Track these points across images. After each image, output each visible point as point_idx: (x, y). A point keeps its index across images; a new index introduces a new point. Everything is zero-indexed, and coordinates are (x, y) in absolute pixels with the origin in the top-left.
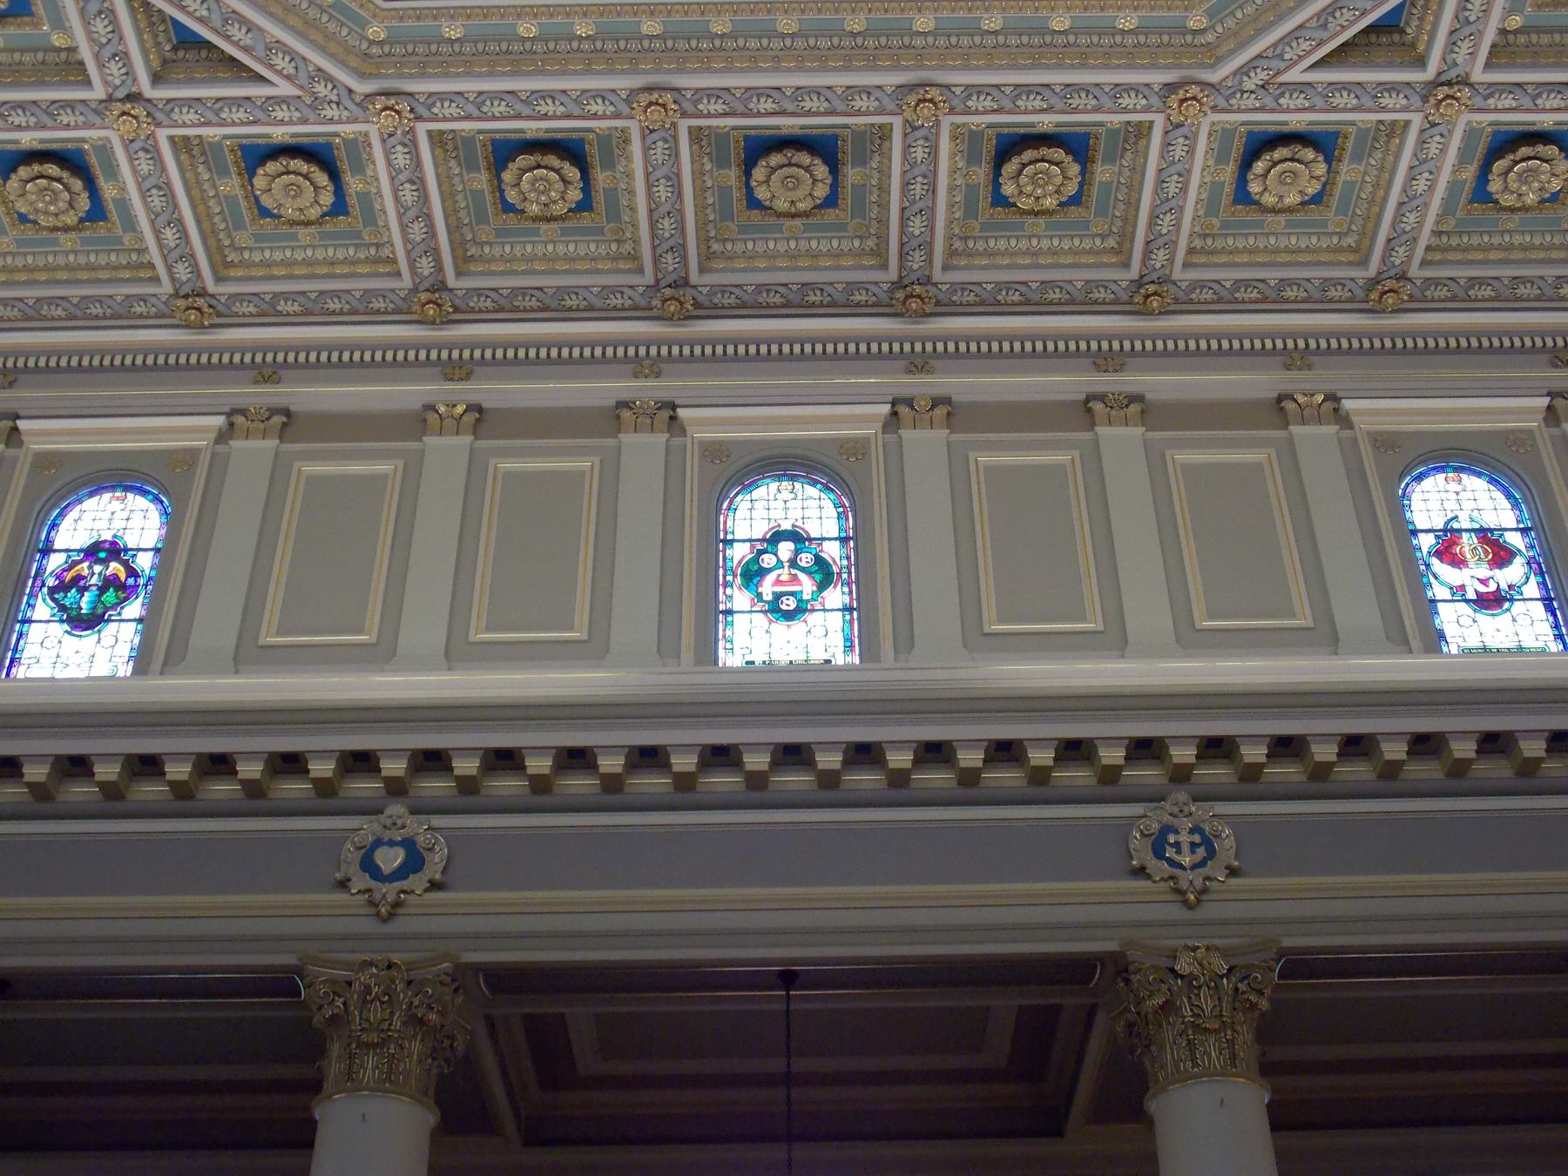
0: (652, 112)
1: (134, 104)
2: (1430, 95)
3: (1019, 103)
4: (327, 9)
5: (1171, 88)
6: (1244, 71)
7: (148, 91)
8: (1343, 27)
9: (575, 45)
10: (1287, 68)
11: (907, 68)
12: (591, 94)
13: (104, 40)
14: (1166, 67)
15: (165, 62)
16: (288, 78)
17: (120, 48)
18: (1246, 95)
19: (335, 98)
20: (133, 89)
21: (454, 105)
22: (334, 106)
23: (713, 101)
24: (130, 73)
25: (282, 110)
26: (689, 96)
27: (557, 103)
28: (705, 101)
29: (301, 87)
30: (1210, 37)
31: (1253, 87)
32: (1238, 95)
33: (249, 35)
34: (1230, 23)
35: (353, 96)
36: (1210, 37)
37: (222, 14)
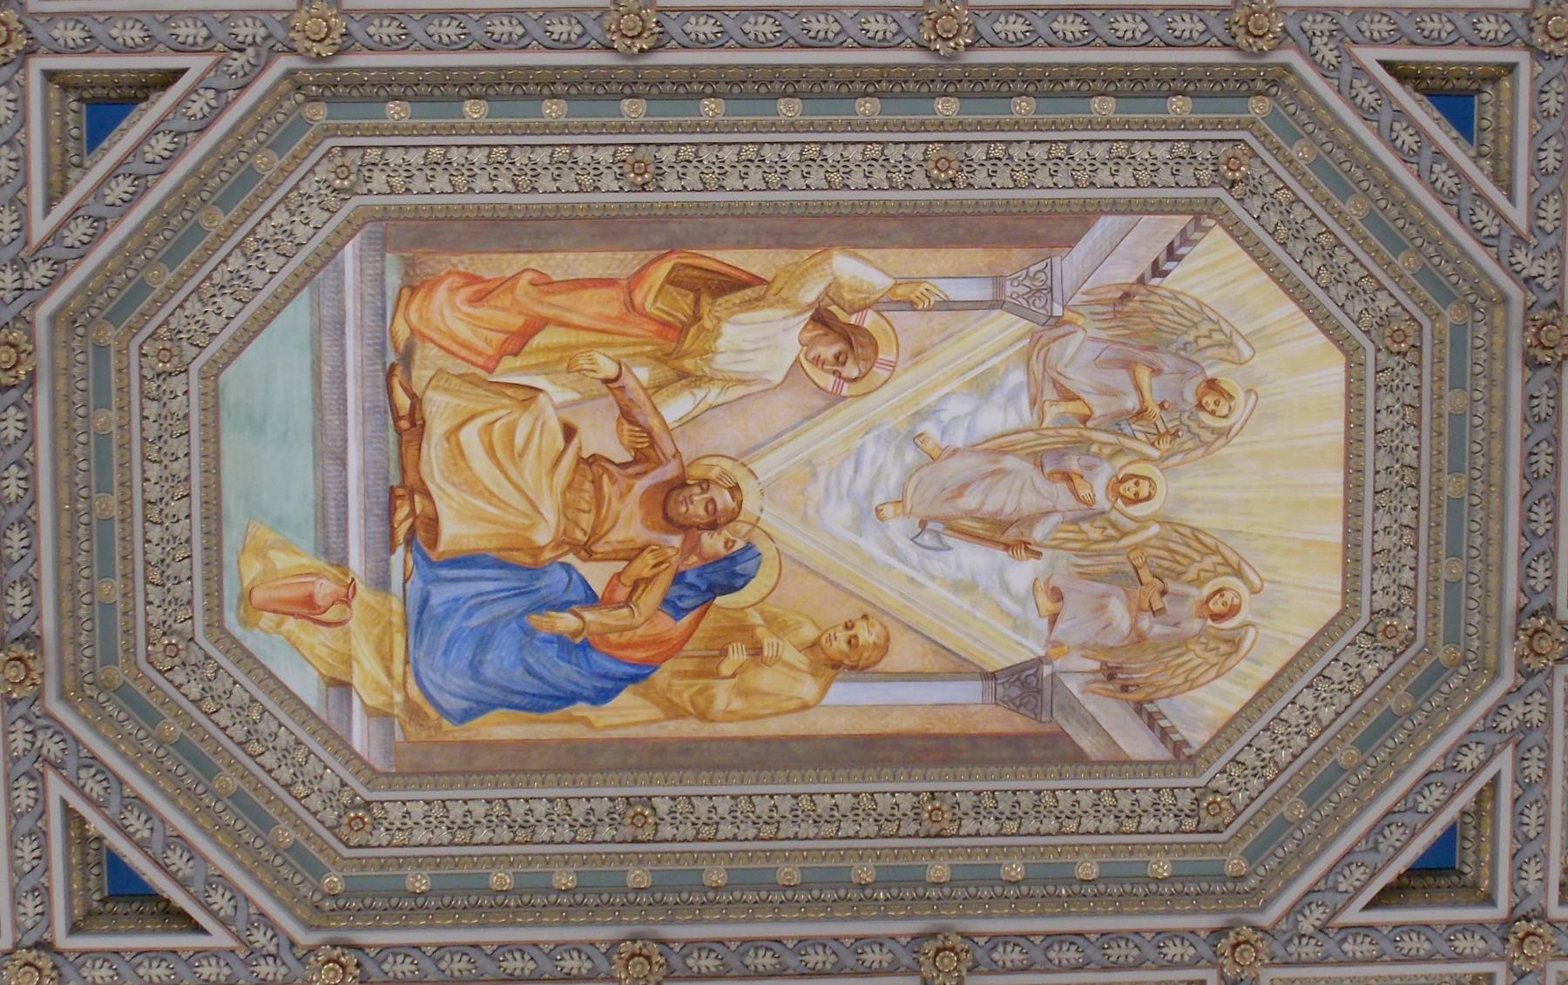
0: (634, 966)
1: (43, 954)
2: (1508, 933)
3: (1052, 954)
4: (281, 851)
5: (1219, 933)
6: (1296, 909)
7: (63, 941)
8: (1396, 849)
9: (553, 898)
10: (1345, 906)
11: (922, 917)
12: (566, 947)
13: (27, 868)
14: (1209, 912)
15: (89, 914)
16: (224, 923)
17: (42, 880)
18: (1304, 941)
19: (272, 949)
20: (46, 936)
21: (408, 960)
22: (270, 960)
23: (704, 954)
24: (45, 914)
25: (210, 965)
26: (677, 950)
27: (527, 957)
28: (695, 955)
29: (237, 937)
30: (1253, 882)
31: (1310, 930)
32: (1296, 941)
33: (191, 863)
34: (1273, 863)
35: (295, 950)
36: (1253, 882)
37: (165, 836)
